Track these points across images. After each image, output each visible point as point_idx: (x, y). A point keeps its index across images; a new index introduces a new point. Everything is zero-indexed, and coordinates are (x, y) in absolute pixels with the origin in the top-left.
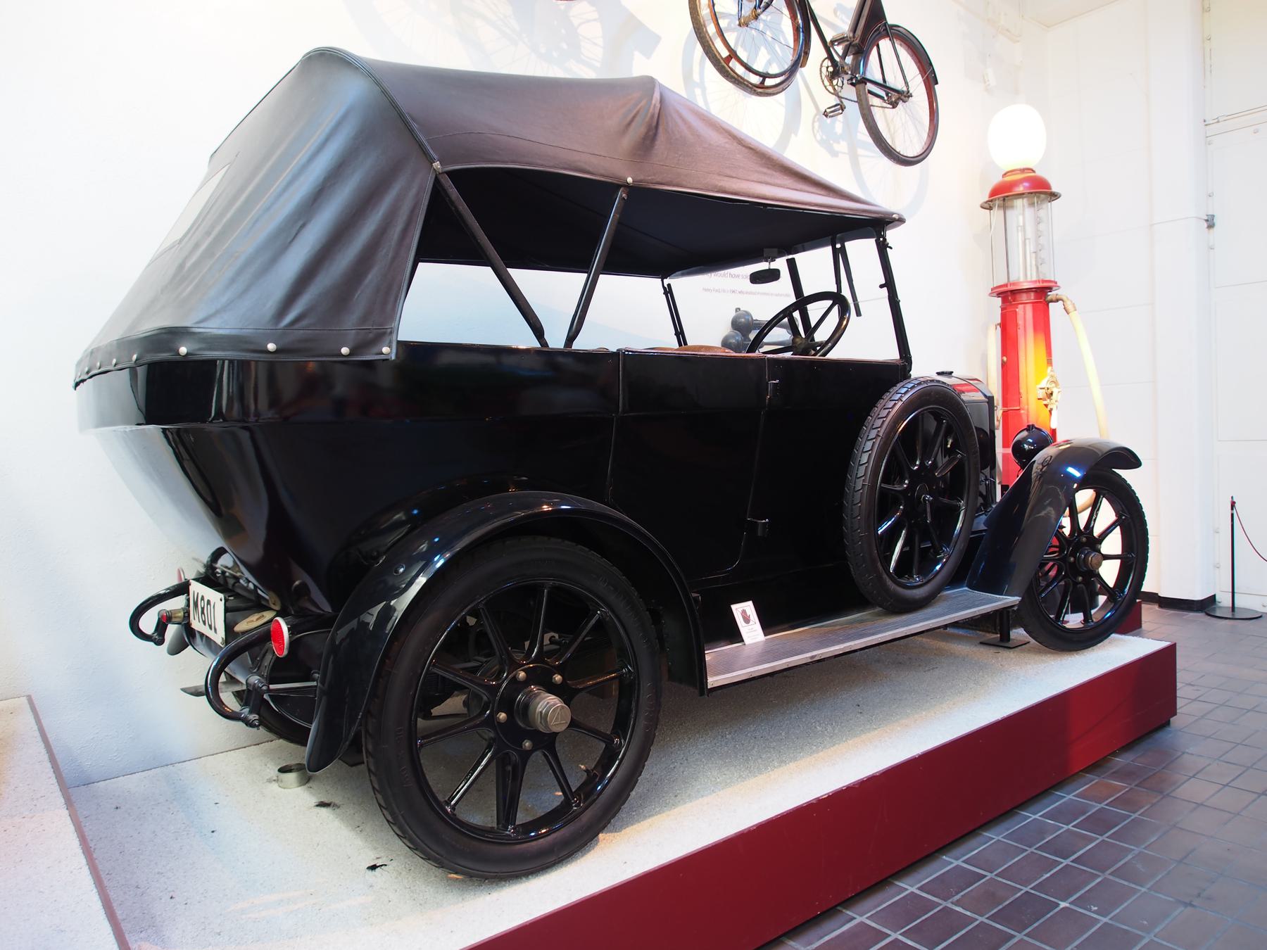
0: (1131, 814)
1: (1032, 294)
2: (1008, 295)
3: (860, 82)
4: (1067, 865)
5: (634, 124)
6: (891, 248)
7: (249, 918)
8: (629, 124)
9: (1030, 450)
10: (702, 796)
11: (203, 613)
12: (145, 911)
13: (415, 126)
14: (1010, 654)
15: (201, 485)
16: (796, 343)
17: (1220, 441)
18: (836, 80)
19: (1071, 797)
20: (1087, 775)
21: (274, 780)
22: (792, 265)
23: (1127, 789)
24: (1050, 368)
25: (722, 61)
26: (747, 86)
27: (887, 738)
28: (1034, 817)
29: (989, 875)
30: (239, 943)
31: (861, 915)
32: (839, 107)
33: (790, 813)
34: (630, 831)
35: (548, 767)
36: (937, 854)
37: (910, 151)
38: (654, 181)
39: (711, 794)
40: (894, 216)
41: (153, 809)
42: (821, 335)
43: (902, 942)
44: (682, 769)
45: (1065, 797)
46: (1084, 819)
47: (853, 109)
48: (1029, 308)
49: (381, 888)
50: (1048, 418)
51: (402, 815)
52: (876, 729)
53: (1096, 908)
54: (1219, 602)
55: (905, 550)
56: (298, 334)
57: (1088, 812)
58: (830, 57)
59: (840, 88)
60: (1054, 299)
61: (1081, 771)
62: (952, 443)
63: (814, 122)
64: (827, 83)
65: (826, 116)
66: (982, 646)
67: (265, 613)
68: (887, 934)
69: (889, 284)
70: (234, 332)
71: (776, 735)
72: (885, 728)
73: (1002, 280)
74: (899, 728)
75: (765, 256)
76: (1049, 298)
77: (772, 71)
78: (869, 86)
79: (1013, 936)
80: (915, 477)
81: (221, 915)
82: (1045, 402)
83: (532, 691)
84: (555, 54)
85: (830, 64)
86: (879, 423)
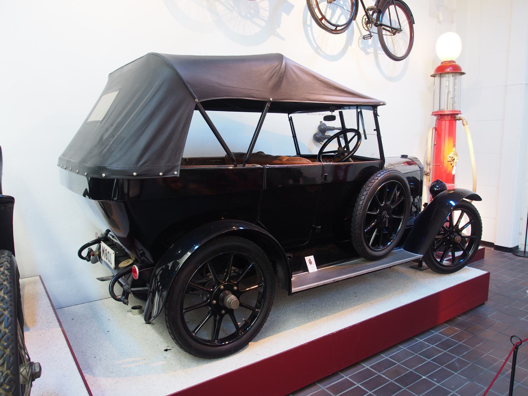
0: (459, 342)
1: (449, 117)
2: (440, 116)
3: (380, 26)
4: (429, 362)
5: (274, 77)
6: (379, 116)
7: (122, 367)
8: (272, 77)
9: (437, 190)
10: (289, 329)
11: (106, 255)
12: (86, 362)
13: (189, 85)
16: (339, 150)
17: (527, 181)
18: (369, 25)
19: (437, 333)
20: (446, 324)
21: (130, 311)
22: (341, 114)
23: (460, 331)
24: (454, 148)
25: (319, 20)
26: (329, 30)
27: (363, 309)
28: (420, 340)
29: (398, 363)
30: (119, 377)
31: (346, 376)
32: (370, 35)
33: (321, 338)
34: (260, 342)
35: (232, 321)
36: (380, 353)
37: (399, 55)
38: (281, 99)
39: (292, 328)
40: (381, 103)
41: (86, 320)
42: (352, 146)
43: (360, 387)
44: (283, 317)
45: (434, 333)
46: (440, 343)
47: (376, 36)
48: (447, 123)
49: (169, 359)
50: (452, 169)
51: (177, 337)
52: (360, 304)
53: (436, 380)
54: (520, 249)
55: (377, 234)
57: (442, 340)
58: (367, 14)
59: (370, 28)
60: (458, 119)
61: (444, 322)
63: (359, 40)
64: (365, 26)
65: (364, 39)
66: (410, 268)
67: (129, 260)
68: (355, 384)
69: (377, 129)
70: (121, 169)
71: (321, 304)
72: (364, 304)
73: (437, 109)
74: (369, 305)
75: (330, 109)
76: (456, 118)
77: (340, 24)
79: (402, 388)
80: (382, 209)
81: (112, 365)
82: (451, 163)
83: (226, 292)
84: (249, 15)
85: (366, 18)
86: (368, 188)
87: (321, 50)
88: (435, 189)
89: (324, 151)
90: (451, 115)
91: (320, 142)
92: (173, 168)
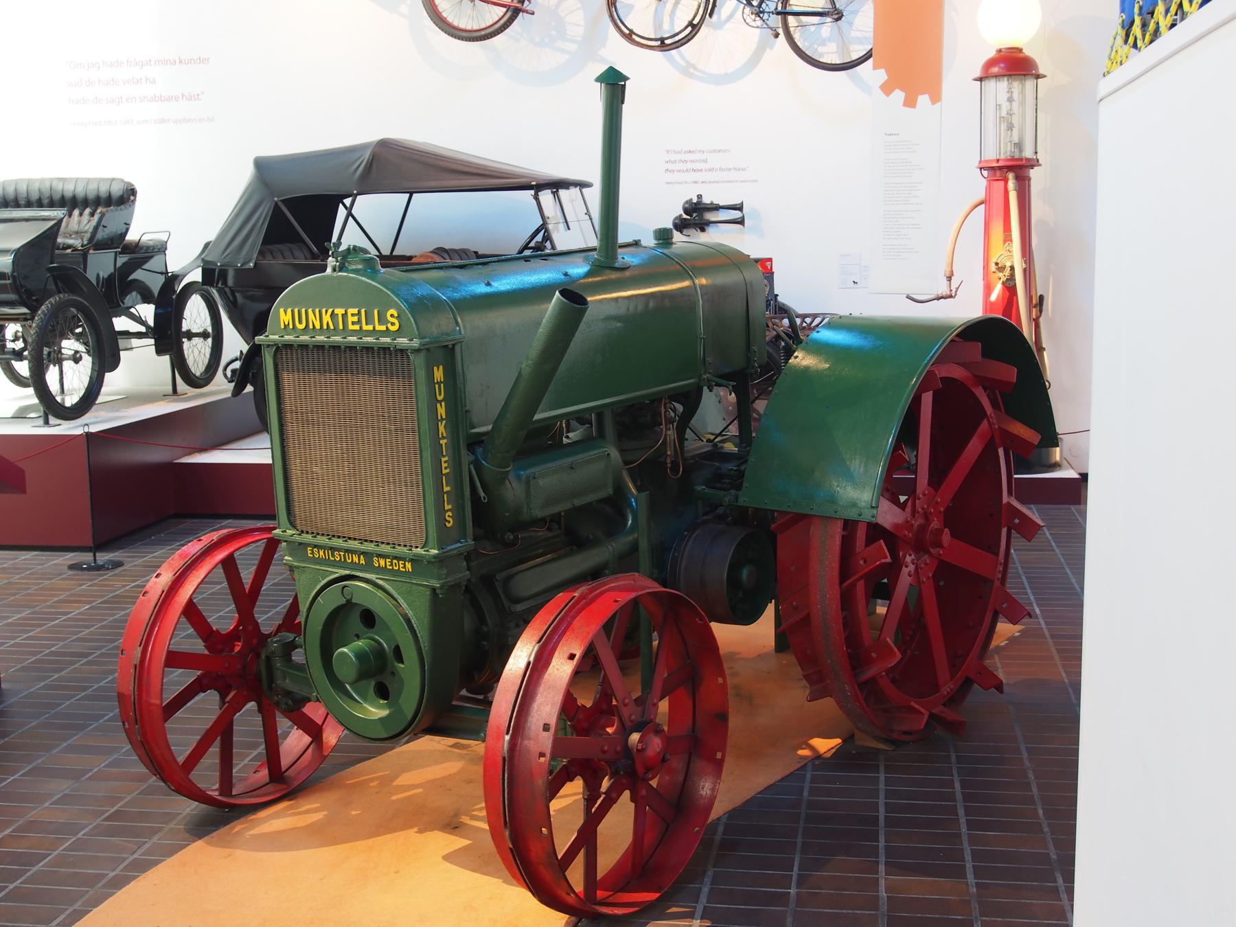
56: (226, 260)
92: (249, 261)
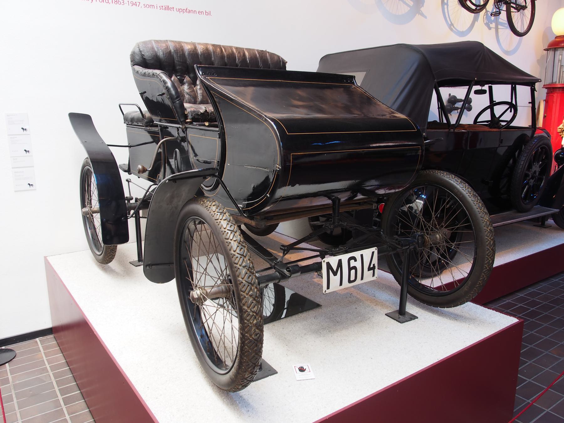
6: (536, 91)
14: (544, 229)
15: (222, 151)
47: (503, 15)
62: (545, 157)
63: (484, 15)
78: (512, 5)
87: (454, 27)
88: (561, 156)
89: (478, 121)
90: (563, 88)
91: (344, 105)
